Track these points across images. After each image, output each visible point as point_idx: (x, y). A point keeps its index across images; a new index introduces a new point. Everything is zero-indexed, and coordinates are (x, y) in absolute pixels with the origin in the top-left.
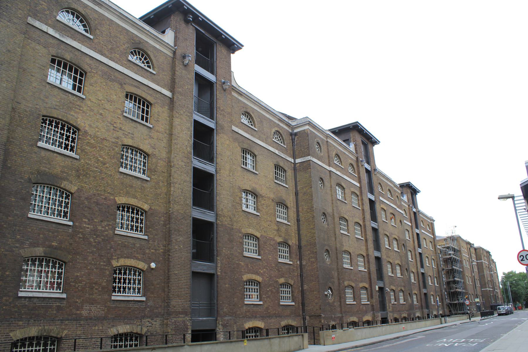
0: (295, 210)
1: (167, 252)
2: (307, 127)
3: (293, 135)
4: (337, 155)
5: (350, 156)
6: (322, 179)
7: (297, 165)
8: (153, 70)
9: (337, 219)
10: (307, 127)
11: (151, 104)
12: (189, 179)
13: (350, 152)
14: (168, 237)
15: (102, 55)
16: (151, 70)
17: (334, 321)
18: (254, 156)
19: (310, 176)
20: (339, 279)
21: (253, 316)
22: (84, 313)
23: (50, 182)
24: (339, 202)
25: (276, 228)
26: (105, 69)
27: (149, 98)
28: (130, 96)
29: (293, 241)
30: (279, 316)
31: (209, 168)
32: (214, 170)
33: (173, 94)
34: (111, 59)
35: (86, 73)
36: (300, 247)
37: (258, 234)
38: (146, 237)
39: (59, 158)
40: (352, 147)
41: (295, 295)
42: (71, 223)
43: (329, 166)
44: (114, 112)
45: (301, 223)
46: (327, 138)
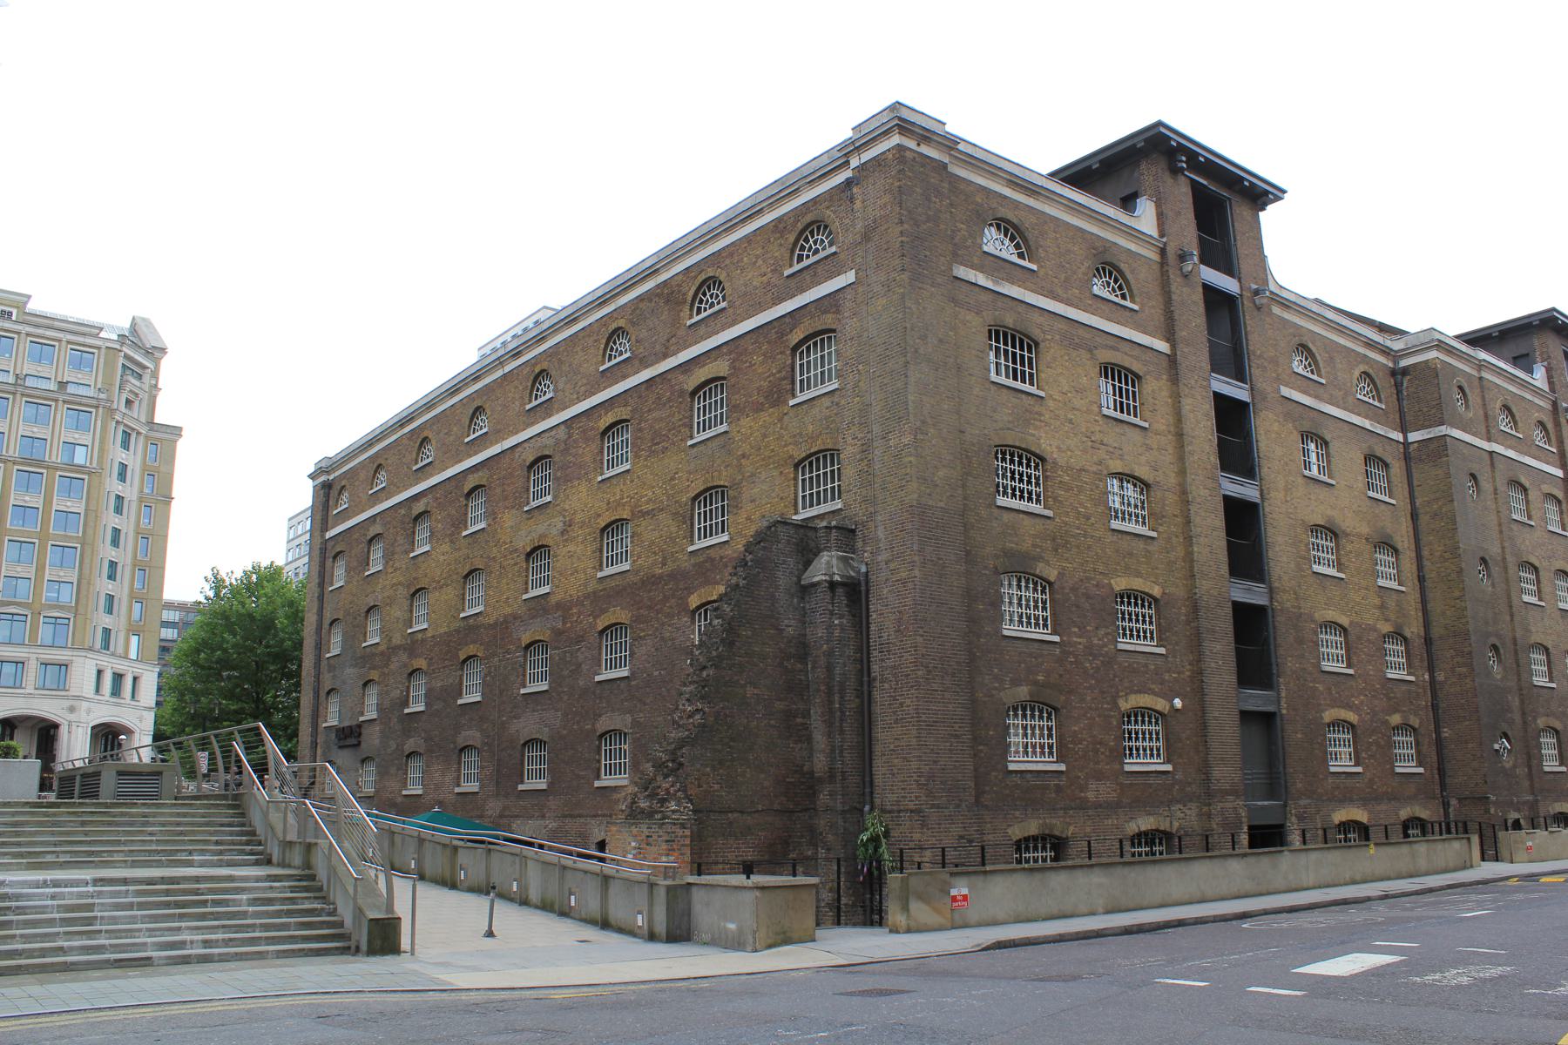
0: (1413, 555)
1: (1198, 674)
2: (1433, 354)
3: (1397, 374)
4: (1506, 408)
5: (1537, 401)
6: (1473, 476)
7: (1412, 448)
8: (1133, 301)
9: (1512, 569)
10: (1433, 354)
11: (1139, 377)
12: (1218, 521)
13: (1537, 391)
14: (1196, 644)
15: (1054, 298)
16: (1127, 303)
17: (1518, 810)
18: (1325, 443)
19: (1448, 475)
20: (1524, 714)
21: (1346, 799)
22: (1091, 795)
23: (1022, 569)
24: (1515, 527)
25: (1377, 601)
26: (1062, 326)
27: (1136, 367)
28: (1108, 370)
29: (1414, 629)
30: (1392, 797)
31: (1249, 492)
32: (1257, 494)
33: (1173, 347)
34: (1069, 303)
35: (1037, 344)
36: (1428, 641)
37: (1344, 621)
38: (1162, 651)
39: (1027, 521)
40: (1539, 377)
41: (1424, 749)
42: (1056, 639)
43: (1489, 440)
44: (1088, 411)
45: (1428, 584)
46: (1479, 371)
